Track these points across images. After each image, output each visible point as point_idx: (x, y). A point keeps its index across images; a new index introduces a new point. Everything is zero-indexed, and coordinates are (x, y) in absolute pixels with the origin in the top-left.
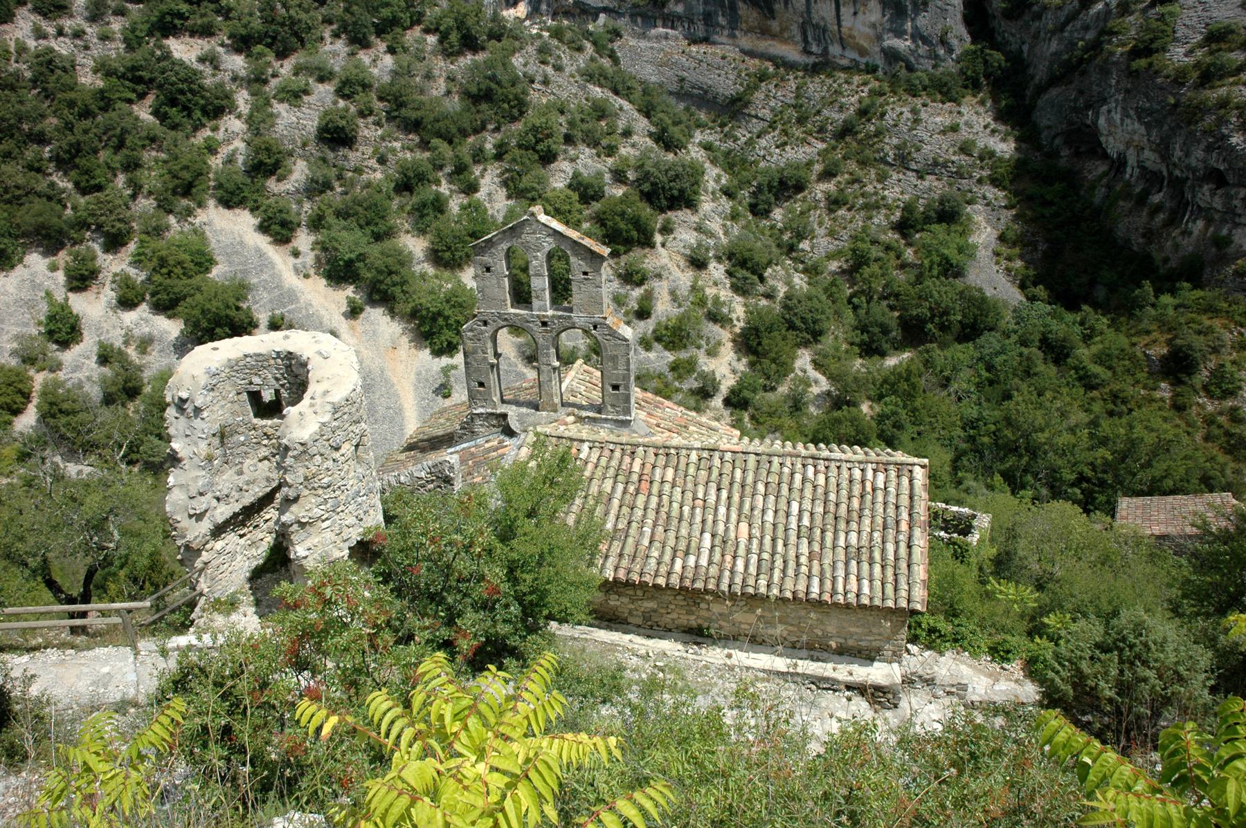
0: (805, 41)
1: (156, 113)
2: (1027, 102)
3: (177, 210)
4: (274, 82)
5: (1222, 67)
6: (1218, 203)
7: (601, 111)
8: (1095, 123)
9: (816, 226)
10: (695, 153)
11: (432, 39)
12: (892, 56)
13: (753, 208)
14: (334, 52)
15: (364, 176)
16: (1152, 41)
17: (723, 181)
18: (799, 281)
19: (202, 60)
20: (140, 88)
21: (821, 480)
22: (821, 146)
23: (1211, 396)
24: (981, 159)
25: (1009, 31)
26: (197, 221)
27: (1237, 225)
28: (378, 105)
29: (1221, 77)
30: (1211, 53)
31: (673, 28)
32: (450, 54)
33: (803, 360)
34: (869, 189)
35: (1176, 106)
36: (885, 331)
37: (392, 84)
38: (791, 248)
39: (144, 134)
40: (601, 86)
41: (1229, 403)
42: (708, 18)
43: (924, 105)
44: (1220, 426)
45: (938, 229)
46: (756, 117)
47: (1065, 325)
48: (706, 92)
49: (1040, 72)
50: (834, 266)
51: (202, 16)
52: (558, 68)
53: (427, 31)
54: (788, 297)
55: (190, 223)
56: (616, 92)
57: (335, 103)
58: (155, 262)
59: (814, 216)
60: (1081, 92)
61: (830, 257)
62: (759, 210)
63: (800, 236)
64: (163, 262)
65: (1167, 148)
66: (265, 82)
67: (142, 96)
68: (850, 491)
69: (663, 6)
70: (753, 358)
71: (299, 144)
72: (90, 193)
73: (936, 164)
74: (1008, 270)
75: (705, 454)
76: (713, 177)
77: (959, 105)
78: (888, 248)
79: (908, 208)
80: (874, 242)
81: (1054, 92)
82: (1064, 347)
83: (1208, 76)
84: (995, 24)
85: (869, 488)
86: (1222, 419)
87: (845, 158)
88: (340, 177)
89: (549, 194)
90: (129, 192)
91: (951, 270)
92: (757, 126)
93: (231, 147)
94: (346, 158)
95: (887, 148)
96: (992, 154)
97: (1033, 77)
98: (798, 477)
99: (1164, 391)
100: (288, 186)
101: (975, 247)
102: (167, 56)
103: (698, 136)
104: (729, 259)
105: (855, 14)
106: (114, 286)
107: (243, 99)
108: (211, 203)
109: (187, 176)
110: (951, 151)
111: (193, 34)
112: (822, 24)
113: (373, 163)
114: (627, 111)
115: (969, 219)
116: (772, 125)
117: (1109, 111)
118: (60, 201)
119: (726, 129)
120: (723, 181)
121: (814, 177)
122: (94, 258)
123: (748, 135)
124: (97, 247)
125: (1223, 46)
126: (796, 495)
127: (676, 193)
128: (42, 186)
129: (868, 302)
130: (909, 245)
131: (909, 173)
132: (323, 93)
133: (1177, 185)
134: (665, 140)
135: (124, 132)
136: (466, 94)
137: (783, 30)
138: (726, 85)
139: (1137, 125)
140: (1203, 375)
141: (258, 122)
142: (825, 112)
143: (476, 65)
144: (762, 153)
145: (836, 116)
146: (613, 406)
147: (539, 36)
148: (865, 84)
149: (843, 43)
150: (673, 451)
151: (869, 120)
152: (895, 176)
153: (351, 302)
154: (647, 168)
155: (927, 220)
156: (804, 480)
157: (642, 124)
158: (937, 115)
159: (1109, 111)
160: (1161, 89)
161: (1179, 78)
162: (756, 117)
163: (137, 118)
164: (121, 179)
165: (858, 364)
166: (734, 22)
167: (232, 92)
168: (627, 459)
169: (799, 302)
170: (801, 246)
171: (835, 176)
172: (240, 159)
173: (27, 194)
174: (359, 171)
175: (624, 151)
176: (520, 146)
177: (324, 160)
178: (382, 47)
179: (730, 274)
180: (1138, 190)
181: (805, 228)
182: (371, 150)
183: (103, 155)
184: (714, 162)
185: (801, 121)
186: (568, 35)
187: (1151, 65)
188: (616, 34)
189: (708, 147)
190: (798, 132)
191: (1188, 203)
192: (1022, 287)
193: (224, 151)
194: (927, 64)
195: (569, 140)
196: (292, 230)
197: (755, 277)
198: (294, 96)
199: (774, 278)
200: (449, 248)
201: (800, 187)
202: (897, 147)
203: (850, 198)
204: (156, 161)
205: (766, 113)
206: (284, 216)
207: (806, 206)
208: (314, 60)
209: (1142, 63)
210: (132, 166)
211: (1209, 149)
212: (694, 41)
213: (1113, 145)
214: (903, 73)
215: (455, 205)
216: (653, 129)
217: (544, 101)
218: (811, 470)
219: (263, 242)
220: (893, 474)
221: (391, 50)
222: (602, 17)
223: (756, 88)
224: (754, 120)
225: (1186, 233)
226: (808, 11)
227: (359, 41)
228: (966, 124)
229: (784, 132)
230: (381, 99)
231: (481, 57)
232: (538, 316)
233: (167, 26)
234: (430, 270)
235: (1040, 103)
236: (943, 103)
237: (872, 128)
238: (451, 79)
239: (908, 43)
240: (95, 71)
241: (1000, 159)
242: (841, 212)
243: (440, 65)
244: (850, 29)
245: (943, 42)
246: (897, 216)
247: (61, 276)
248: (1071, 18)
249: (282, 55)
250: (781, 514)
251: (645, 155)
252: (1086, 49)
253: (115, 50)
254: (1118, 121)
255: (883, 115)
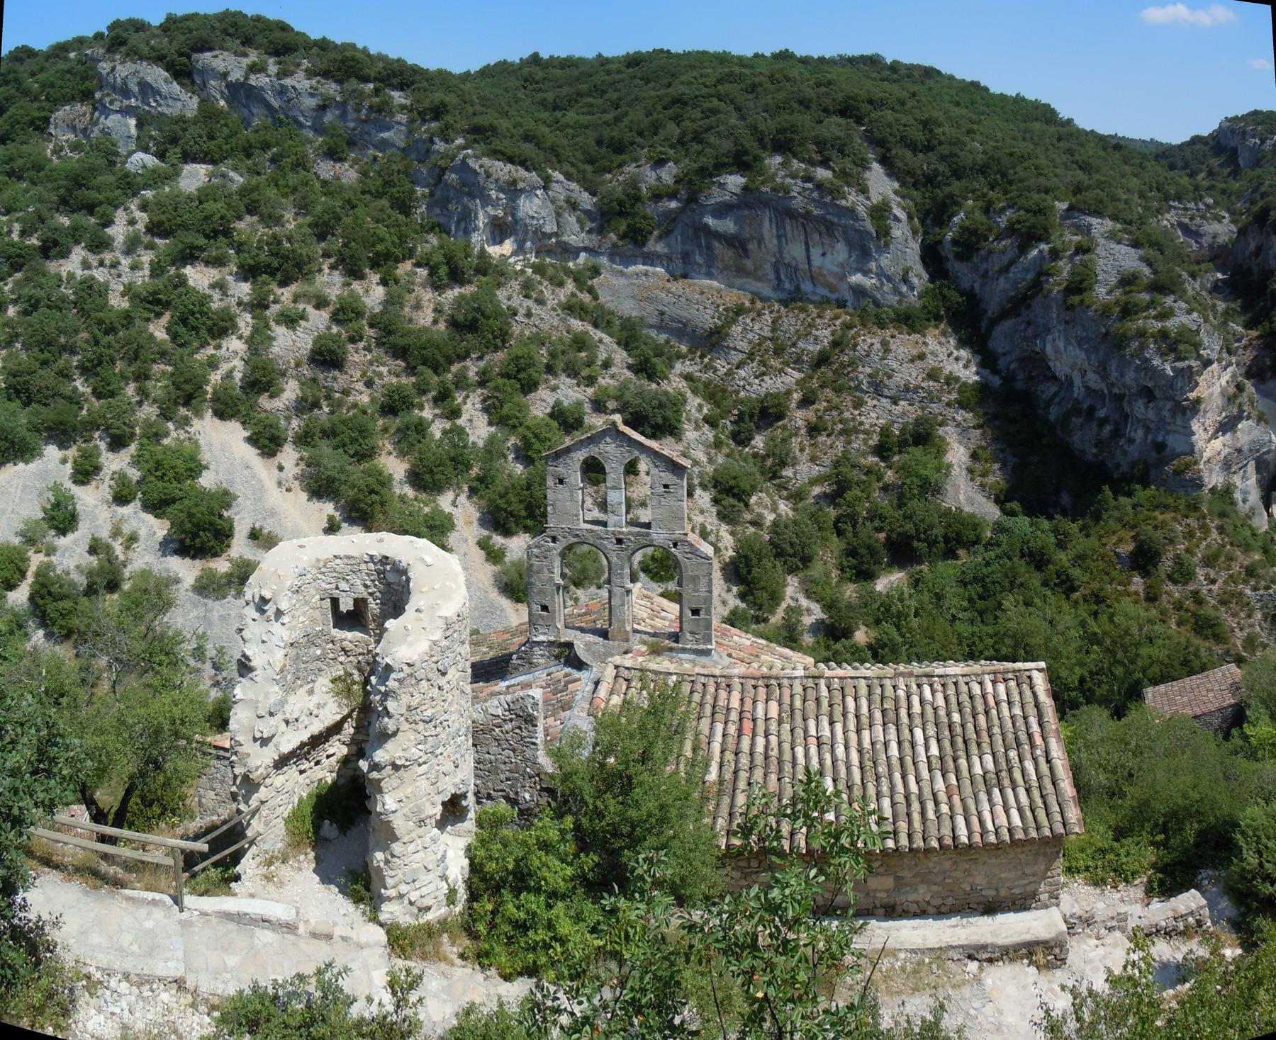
0: (778, 278)
1: (168, 330)
2: (983, 330)
3: (177, 418)
4: (275, 308)
5: (1136, 305)
6: (1151, 415)
7: (580, 343)
8: (1043, 350)
9: (798, 453)
10: (675, 384)
11: (423, 272)
12: (859, 291)
13: (735, 436)
14: (331, 283)
15: (351, 399)
16: (1081, 282)
17: (705, 411)
18: (784, 508)
19: (212, 286)
20: (157, 309)
21: (940, 701)
22: (798, 375)
23: (1175, 582)
24: (948, 383)
25: (957, 267)
26: (192, 430)
27: (1168, 432)
28: (371, 332)
29: (1136, 313)
30: (1126, 293)
31: (652, 265)
32: (438, 287)
33: (792, 588)
34: (847, 415)
35: (1106, 334)
36: (872, 551)
37: (382, 313)
38: (775, 476)
39: (156, 349)
40: (582, 320)
41: (1191, 588)
42: (686, 256)
43: (893, 337)
44: (1187, 610)
45: (917, 452)
46: (735, 349)
47: (1039, 531)
48: (685, 325)
49: (993, 308)
50: (817, 490)
51: (217, 248)
52: (540, 302)
53: (418, 265)
54: (775, 524)
55: (187, 432)
56: (596, 326)
57: (329, 328)
58: (152, 464)
59: (795, 442)
60: (1029, 323)
61: (813, 482)
62: (741, 439)
63: (783, 464)
64: (158, 465)
65: (1105, 369)
66: (267, 307)
67: (159, 315)
68: (973, 708)
69: (644, 244)
70: (742, 588)
71: (292, 365)
72: (105, 397)
73: (907, 389)
74: (982, 485)
75: (810, 683)
76: (695, 405)
77: (924, 336)
78: (869, 472)
79: (885, 432)
80: (853, 466)
81: (1007, 325)
82: (1043, 554)
83: (1128, 311)
84: (949, 266)
85: (992, 702)
86: (1189, 603)
87: (822, 387)
88: (328, 397)
89: (529, 423)
90: (138, 399)
91: (930, 488)
92: (736, 357)
93: (231, 365)
94: (335, 379)
95: (861, 376)
96: (957, 379)
97: (985, 311)
98: (916, 700)
99: (1137, 583)
100: (278, 404)
101: (950, 466)
102: (183, 281)
103: (679, 367)
104: (715, 487)
105: (824, 254)
106: (112, 483)
107: (245, 322)
108: (209, 414)
109: (187, 387)
110: (920, 378)
111: (207, 263)
112: (794, 263)
113: (360, 386)
114: (606, 344)
115: (942, 439)
116: (751, 356)
117: (1054, 340)
118: (78, 403)
119: (706, 360)
120: (705, 411)
121: (793, 405)
122: (99, 455)
123: (728, 367)
124: (102, 445)
125: (1133, 288)
126: (918, 721)
127: (660, 421)
128: (66, 389)
129: (854, 527)
130: (890, 467)
131: (884, 400)
132: (318, 319)
133: (1119, 398)
134: (644, 368)
135: (140, 347)
136: (454, 324)
137: (756, 269)
138: (707, 318)
139: (1078, 352)
140: (1166, 564)
141: (258, 342)
142: (801, 344)
143: (462, 297)
144: (742, 383)
145: (811, 348)
146: (692, 633)
147: (523, 272)
148: (836, 318)
149: (813, 279)
150: (773, 682)
151: (842, 351)
152: (870, 403)
153: (331, 519)
154: (628, 396)
155: (903, 444)
156: (922, 702)
157: (620, 356)
158: (903, 345)
159: (1054, 340)
160: (1094, 321)
161: (1105, 312)
162: (735, 349)
163: (151, 335)
164: (131, 389)
165: (850, 592)
166: (711, 259)
167: (236, 316)
168: (723, 694)
169: (786, 527)
170: (784, 473)
171: (813, 403)
172: (238, 376)
173: (53, 396)
174: (346, 392)
175: (604, 381)
176: (503, 375)
177: (314, 380)
178: (376, 278)
179: (716, 501)
180: (1085, 406)
181: (787, 454)
182: (358, 374)
183: (119, 365)
184: (695, 392)
185: (778, 352)
186: (550, 272)
187: (1082, 301)
188: (596, 271)
189: (688, 377)
190: (775, 363)
191: (1127, 416)
192: (997, 501)
193: (224, 367)
194: (893, 299)
195: (550, 369)
196: (280, 445)
197: (742, 505)
198: (291, 320)
199: (759, 504)
200: (431, 471)
201: (780, 416)
202: (870, 376)
203: (829, 424)
204: (164, 373)
205: (744, 345)
206: (272, 431)
207: (786, 434)
208: (311, 289)
209: (1075, 299)
210: (142, 376)
211: (1138, 369)
212: (674, 277)
213: (1061, 368)
214: (871, 308)
215: (437, 430)
216: (630, 360)
217: (527, 333)
218: (927, 689)
219: (251, 453)
220: (1012, 684)
221: (384, 282)
222: (583, 255)
223: (734, 321)
224: (733, 352)
225: (1131, 441)
226: (781, 251)
227: (354, 273)
228: (932, 353)
229: (763, 363)
230: (371, 326)
231: (468, 290)
232: (613, 533)
233: (188, 256)
234: (410, 492)
235: (994, 333)
236: (909, 334)
237: (846, 358)
238: (438, 310)
239: (873, 281)
240: (123, 295)
241: (965, 384)
242: (822, 438)
243: (428, 296)
244: (820, 268)
245: (905, 280)
246: (874, 441)
247: (69, 469)
248: (1012, 263)
249: (284, 283)
250: (907, 745)
251: (624, 387)
252: (1029, 289)
253: (142, 278)
254: (1062, 348)
255: (856, 345)
